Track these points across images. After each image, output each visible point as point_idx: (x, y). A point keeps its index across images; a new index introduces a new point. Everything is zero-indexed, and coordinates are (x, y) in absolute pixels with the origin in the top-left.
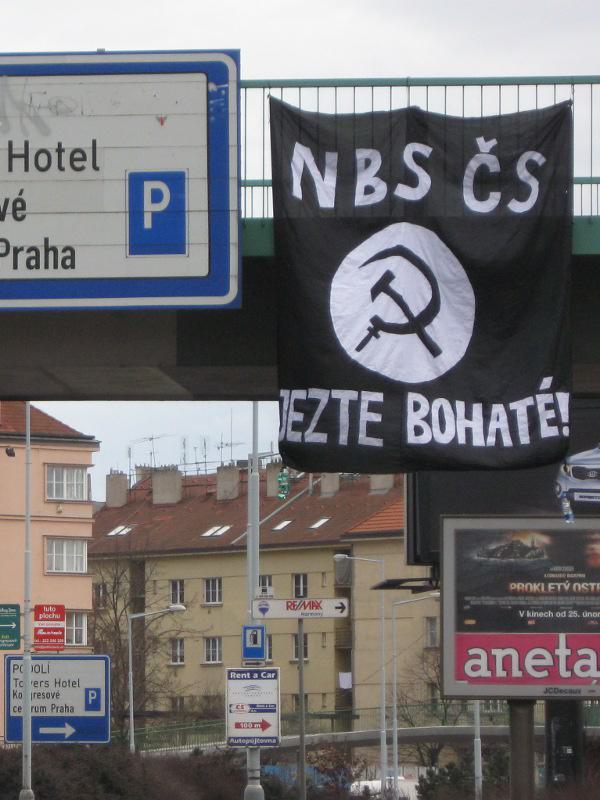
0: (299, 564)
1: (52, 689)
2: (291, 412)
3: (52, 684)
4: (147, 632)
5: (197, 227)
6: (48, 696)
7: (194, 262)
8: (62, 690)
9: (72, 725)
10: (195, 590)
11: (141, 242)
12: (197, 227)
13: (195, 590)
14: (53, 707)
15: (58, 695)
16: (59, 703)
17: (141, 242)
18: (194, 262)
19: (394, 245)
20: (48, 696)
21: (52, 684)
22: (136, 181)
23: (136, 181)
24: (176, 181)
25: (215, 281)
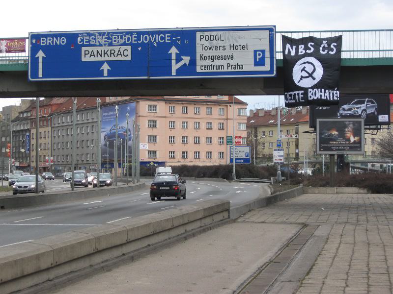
1: (228, 53)
3: (228, 48)
5: (267, 61)
7: (267, 68)
11: (256, 64)
12: (267, 61)
15: (232, 57)
17: (256, 64)
18: (267, 68)
21: (228, 48)
22: (255, 52)
23: (255, 52)
24: (263, 51)
25: (271, 72)
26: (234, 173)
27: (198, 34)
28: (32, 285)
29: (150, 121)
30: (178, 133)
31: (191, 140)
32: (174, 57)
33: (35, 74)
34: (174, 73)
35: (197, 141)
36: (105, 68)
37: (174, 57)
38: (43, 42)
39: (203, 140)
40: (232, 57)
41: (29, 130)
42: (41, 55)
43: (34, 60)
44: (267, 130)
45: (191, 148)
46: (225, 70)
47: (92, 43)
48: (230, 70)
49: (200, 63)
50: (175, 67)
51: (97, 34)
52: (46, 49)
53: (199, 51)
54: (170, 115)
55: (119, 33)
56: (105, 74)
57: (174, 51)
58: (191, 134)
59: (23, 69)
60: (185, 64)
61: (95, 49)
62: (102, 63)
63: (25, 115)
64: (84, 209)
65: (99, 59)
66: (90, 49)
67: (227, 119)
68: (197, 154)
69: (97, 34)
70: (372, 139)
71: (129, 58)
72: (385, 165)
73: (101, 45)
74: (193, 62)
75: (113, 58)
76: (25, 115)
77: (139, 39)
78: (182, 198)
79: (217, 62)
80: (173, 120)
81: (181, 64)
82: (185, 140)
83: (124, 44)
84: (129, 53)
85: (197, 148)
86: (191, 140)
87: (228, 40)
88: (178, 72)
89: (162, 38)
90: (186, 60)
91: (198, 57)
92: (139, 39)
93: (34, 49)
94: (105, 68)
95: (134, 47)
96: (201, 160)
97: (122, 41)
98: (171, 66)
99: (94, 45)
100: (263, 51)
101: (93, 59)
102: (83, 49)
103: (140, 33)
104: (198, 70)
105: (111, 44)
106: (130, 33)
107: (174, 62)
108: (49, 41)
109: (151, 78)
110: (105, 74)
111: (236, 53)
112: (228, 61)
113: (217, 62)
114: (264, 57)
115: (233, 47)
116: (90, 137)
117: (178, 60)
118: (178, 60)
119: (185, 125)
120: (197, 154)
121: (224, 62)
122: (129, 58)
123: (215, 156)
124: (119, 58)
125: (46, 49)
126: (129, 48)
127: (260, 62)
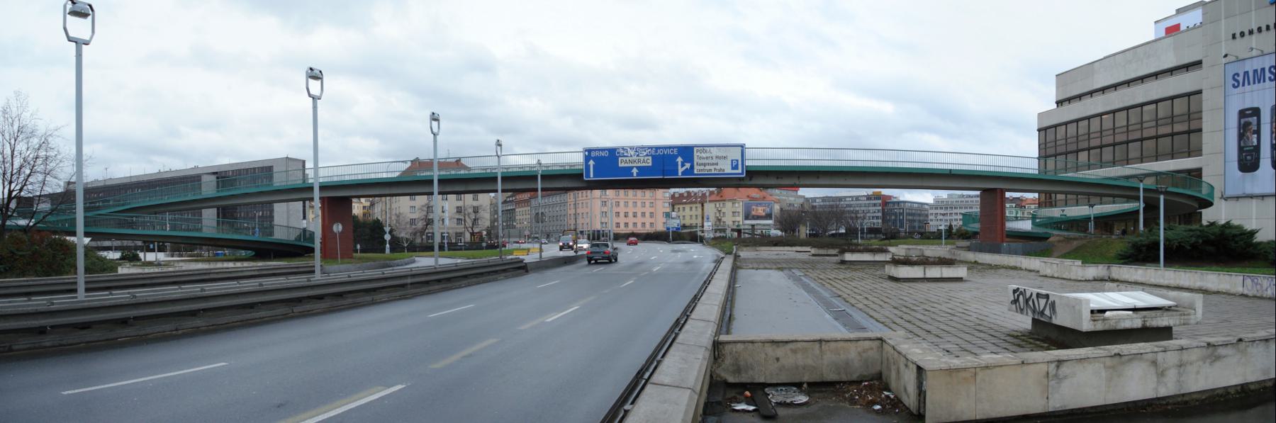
0: (691, 205)
1: (714, 161)
2: (629, 197)
3: (714, 158)
4: (911, 409)
5: (740, 166)
6: (713, 164)
7: (740, 171)
8: (719, 161)
9: (589, 161)
10: (681, 209)
11: (733, 168)
12: (740, 166)
13: (681, 209)
14: (715, 169)
15: (717, 164)
16: (718, 167)
17: (733, 168)
18: (740, 171)
19: (75, 58)
20: (713, 164)
21: (714, 158)
22: (732, 161)
23: (732, 161)
24: (737, 161)
25: (742, 174)
26: (671, 237)
27: (695, 149)
28: (710, 289)
29: (634, 202)
30: (622, 209)
31: (631, 215)
32: (680, 163)
33: (588, 175)
34: (680, 174)
35: (626, 215)
36: (635, 171)
37: (680, 163)
38: (593, 154)
39: (639, 215)
40: (717, 164)
41: (514, 209)
42: (591, 163)
43: (587, 167)
44: (681, 207)
45: (631, 220)
46: (713, 172)
47: (625, 154)
48: (716, 172)
49: (696, 168)
50: (681, 170)
51: (629, 149)
52: (595, 159)
53: (696, 160)
54: (625, 197)
55: (643, 148)
56: (635, 175)
57: (680, 160)
58: (639, 210)
59: (580, 172)
60: (687, 169)
61: (627, 159)
62: (632, 168)
63: (511, 199)
64: (1114, 198)
65: (630, 165)
66: (624, 159)
67: (656, 199)
68: (635, 224)
69: (629, 149)
70: (457, 219)
71: (650, 164)
72: (764, 231)
73: (631, 156)
74: (692, 167)
75: (639, 165)
76: (511, 199)
77: (656, 152)
78: (613, 261)
79: (707, 167)
80: (644, 201)
81: (684, 168)
82: (643, 214)
83: (647, 155)
84: (650, 161)
85: (635, 220)
86: (631, 215)
87: (715, 152)
88: (683, 173)
89: (672, 151)
90: (688, 165)
91: (695, 164)
92: (656, 152)
93: (587, 159)
94: (635, 171)
95: (654, 157)
96: (621, 229)
97: (645, 154)
98: (678, 170)
99: (627, 156)
100: (737, 161)
101: (626, 165)
102: (620, 159)
103: (657, 148)
104: (696, 172)
105: (638, 156)
106: (651, 148)
107: (680, 167)
108: (597, 154)
109: (666, 177)
110: (635, 175)
111: (719, 161)
112: (716, 167)
113: (707, 167)
114: (737, 164)
115: (717, 157)
116: (563, 213)
117: (683, 166)
118: (683, 166)
119: (626, 204)
120: (635, 224)
121: (712, 167)
122: (650, 164)
123: (648, 226)
124: (644, 164)
125: (595, 159)
126: (650, 158)
127: (735, 167)
